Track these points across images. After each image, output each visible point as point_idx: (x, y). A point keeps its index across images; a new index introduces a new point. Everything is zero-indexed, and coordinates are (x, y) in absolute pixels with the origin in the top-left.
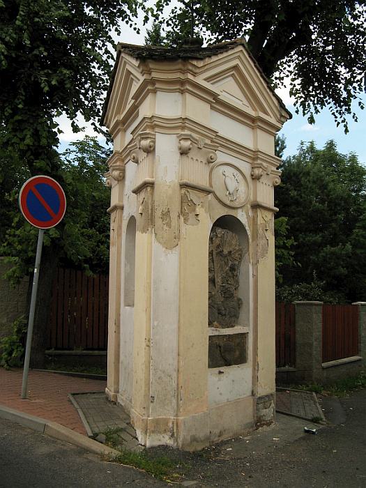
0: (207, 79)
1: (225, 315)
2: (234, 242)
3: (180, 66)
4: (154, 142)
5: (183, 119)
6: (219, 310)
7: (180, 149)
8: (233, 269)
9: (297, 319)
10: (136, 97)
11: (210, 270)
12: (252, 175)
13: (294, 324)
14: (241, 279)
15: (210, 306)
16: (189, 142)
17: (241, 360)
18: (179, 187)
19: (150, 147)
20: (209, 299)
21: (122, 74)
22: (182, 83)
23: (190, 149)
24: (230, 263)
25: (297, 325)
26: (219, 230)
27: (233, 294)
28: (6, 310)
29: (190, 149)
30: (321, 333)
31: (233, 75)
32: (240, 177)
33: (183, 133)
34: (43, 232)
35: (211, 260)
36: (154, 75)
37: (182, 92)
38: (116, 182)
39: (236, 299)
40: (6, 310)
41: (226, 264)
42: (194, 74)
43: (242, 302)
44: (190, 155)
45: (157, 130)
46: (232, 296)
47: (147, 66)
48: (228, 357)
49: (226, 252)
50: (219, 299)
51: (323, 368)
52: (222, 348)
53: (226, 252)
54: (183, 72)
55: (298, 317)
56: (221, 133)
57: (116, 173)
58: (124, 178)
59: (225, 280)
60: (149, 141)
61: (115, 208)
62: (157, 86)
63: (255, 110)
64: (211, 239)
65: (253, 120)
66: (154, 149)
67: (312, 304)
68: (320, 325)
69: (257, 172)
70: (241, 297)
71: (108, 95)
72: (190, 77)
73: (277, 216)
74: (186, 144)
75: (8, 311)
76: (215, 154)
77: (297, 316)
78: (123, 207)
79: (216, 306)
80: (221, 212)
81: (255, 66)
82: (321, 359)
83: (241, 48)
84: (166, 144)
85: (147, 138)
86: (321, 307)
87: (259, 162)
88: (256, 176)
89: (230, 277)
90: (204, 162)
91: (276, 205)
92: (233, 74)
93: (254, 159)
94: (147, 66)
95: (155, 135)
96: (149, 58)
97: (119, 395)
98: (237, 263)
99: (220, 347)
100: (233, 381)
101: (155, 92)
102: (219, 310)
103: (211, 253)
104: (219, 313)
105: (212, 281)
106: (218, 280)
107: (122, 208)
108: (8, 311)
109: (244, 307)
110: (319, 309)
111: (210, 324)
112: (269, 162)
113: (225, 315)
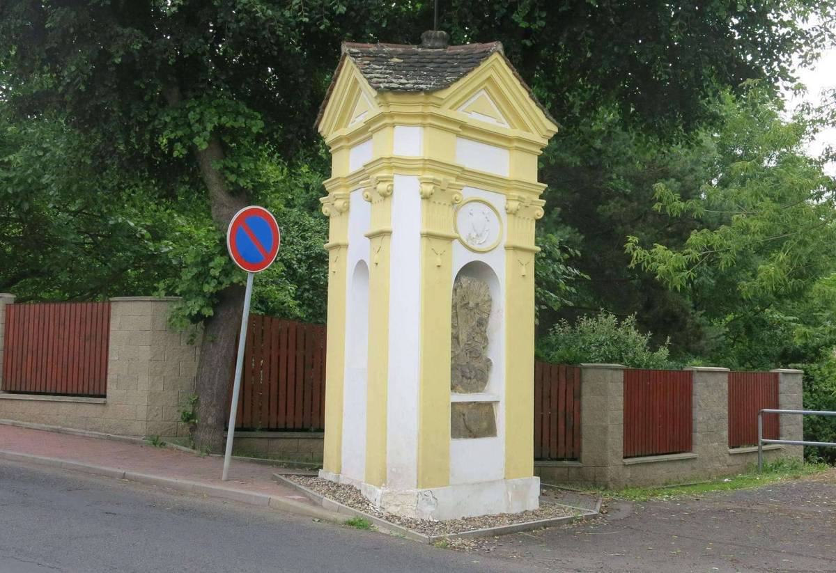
1: (470, 378)
3: (422, 100)
4: (392, 185)
5: (425, 160)
6: (463, 372)
7: (421, 193)
9: (584, 391)
11: (453, 327)
13: (580, 396)
15: (453, 368)
16: (432, 186)
17: (490, 431)
18: (419, 236)
19: (388, 191)
20: (452, 358)
21: (347, 84)
24: (477, 318)
26: (464, 280)
27: (480, 354)
28: (162, 372)
31: (486, 89)
34: (253, 275)
35: (455, 316)
39: (484, 359)
40: (162, 372)
42: (438, 106)
43: (491, 363)
44: (432, 199)
45: (394, 171)
48: (474, 428)
49: (471, 304)
52: (466, 417)
54: (426, 105)
55: (586, 389)
56: (468, 166)
57: (339, 203)
58: (348, 209)
59: (471, 337)
60: (388, 184)
61: (337, 246)
63: (512, 126)
64: (455, 290)
68: (620, 400)
70: (489, 357)
74: (429, 188)
75: (165, 374)
77: (584, 385)
78: (452, 389)
80: (466, 258)
82: (621, 454)
84: (408, 188)
86: (622, 373)
90: (448, 204)
91: (537, 244)
94: (384, 98)
95: (393, 177)
96: (387, 91)
97: (341, 476)
98: (485, 316)
99: (464, 415)
100: (377, 264)
101: (393, 125)
102: (463, 372)
103: (454, 306)
104: (463, 376)
105: (455, 338)
106: (463, 337)
108: (165, 374)
111: (453, 388)
112: (530, 192)
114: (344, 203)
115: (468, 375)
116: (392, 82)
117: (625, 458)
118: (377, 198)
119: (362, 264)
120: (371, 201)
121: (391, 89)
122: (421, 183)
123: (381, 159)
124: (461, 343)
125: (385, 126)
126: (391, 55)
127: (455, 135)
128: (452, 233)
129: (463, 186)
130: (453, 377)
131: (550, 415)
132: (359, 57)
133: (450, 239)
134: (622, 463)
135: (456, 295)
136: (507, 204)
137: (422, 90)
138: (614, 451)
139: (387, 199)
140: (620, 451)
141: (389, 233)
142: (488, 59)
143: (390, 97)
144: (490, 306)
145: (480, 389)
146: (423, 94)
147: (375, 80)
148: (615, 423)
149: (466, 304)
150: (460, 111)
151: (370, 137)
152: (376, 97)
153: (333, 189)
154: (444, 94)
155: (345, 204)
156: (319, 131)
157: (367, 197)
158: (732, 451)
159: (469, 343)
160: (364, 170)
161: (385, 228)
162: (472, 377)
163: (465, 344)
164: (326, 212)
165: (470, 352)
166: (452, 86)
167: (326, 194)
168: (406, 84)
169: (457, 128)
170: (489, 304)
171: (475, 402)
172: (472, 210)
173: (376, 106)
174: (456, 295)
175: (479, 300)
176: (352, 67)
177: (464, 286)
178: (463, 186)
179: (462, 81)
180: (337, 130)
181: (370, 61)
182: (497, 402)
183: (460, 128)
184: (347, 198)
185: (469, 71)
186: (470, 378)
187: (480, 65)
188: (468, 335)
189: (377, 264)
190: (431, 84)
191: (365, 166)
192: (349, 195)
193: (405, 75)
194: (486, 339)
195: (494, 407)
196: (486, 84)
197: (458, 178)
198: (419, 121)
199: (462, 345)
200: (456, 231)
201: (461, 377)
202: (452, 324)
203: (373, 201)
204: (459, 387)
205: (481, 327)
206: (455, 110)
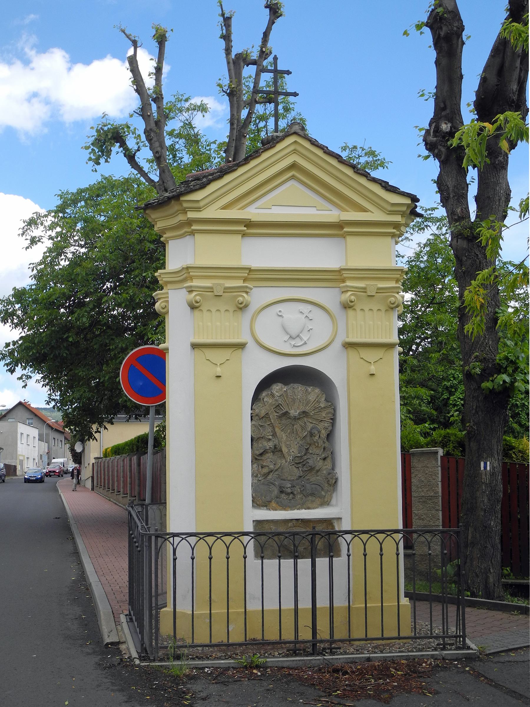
4: (167, 302)
18: (189, 347)
24: (309, 426)
56: (255, 264)
65: (339, 226)
72: (191, 215)
87: (349, 283)
127: (240, 236)
197: (245, 280)
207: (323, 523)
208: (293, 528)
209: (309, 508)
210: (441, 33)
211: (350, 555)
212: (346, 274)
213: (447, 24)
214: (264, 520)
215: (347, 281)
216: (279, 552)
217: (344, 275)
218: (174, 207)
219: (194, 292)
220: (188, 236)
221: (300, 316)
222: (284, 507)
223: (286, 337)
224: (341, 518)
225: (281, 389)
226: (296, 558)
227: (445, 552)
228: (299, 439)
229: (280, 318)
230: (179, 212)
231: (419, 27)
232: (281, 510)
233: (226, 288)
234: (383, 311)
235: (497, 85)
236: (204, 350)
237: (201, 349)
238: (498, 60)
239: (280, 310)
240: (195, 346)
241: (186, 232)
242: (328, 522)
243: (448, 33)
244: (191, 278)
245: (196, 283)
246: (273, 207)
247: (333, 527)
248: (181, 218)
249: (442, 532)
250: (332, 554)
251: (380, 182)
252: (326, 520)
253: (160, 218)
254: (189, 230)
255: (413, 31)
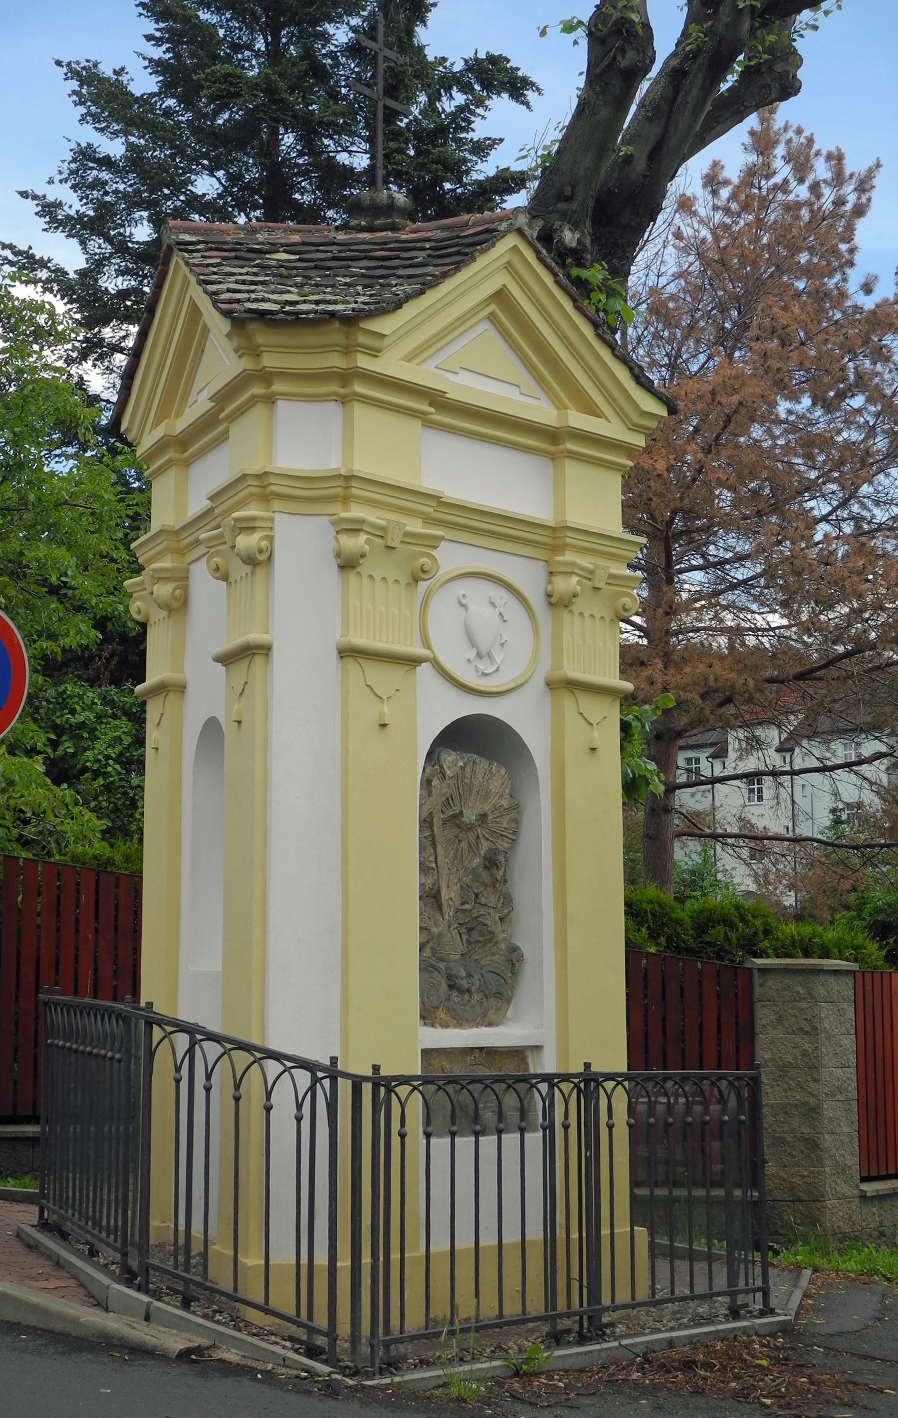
0: (410, 358)
2: (495, 785)
4: (271, 539)
6: (450, 977)
7: (338, 555)
8: (491, 862)
10: (223, 397)
11: (424, 868)
12: (549, 596)
14: (521, 892)
15: (426, 967)
18: (335, 654)
19: (261, 552)
22: (345, 377)
23: (363, 556)
24: (485, 846)
25: (761, 1040)
26: (450, 759)
29: (363, 556)
30: (852, 1073)
32: (514, 609)
33: (344, 515)
36: (270, 361)
37: (345, 400)
38: (164, 613)
39: (503, 946)
41: (473, 849)
45: (277, 505)
46: (490, 938)
47: (248, 337)
49: (470, 815)
50: (454, 946)
51: (864, 1197)
53: (470, 815)
56: (453, 493)
57: (163, 590)
61: (162, 689)
62: (277, 387)
63: (560, 406)
64: (427, 783)
65: (553, 435)
66: (270, 557)
67: (817, 971)
68: (849, 1042)
69: (565, 585)
71: (142, 336)
72: (364, 362)
73: (628, 700)
76: (432, 557)
78: (423, 1017)
79: (442, 965)
81: (558, 283)
83: (511, 241)
85: (253, 529)
86: (850, 981)
87: (569, 556)
88: (561, 598)
89: (485, 885)
92: (492, 314)
93: (556, 549)
95: (272, 520)
96: (251, 319)
98: (503, 844)
100: (239, 722)
101: (270, 400)
102: (450, 977)
103: (426, 823)
104: (451, 987)
107: (181, 688)
109: (528, 971)
110: (845, 988)
111: (428, 1017)
113: (469, 991)
114: (175, 589)
115: (465, 984)
116: (263, 300)
117: (864, 1180)
118: (240, 570)
119: (212, 727)
120: (226, 578)
121: (262, 316)
122: (337, 533)
123: (244, 476)
124: (445, 907)
125: (253, 401)
126: (274, 248)
127: (418, 424)
128: (418, 650)
129: (442, 538)
130: (426, 990)
131: (115, 987)
132: (198, 251)
133: (413, 662)
134: (856, 1192)
135: (430, 795)
136: (550, 582)
137: (333, 315)
138: (837, 1164)
139: (260, 571)
140: (852, 1161)
141: (266, 649)
142: (493, 245)
143: (262, 336)
144: (517, 822)
145: (491, 1016)
146: (337, 325)
147: (225, 296)
148: (839, 1097)
149: (454, 816)
150: (430, 366)
151: (224, 437)
152: (228, 335)
153: (151, 560)
154: (385, 325)
155: (178, 592)
156: (122, 430)
157: (217, 569)
158: (870, 1188)
159: (467, 907)
160: (211, 510)
161: (256, 636)
162: (473, 989)
163: (458, 911)
164: (139, 612)
165: (470, 930)
166: (406, 307)
167: (138, 570)
168: (297, 303)
169: (424, 407)
170: (513, 815)
171: (481, 1049)
172: (464, 596)
173: (233, 356)
174: (430, 795)
175: (487, 808)
176: (186, 277)
177: (449, 773)
178: (442, 538)
179: (431, 297)
180: (157, 425)
181: (224, 258)
182: (538, 1048)
183: (430, 405)
184: (182, 579)
185: (445, 275)
186: (469, 991)
187: (474, 259)
188: (462, 888)
189: (239, 722)
190: (356, 302)
191: (212, 498)
192: (188, 571)
193: (300, 286)
194: (507, 900)
195: (530, 1060)
196: (492, 307)
197: (428, 520)
198: (334, 388)
199: (449, 912)
200: (427, 644)
201: (444, 987)
202: (421, 864)
203: (232, 580)
204: (441, 1014)
205: (494, 871)
206: (418, 364)
207: (514, 1057)
208: (475, 1067)
209: (490, 1024)
210: (619, 59)
211: (569, 1126)
212: (571, 539)
213: (640, 48)
214: (432, 1050)
215: (567, 553)
216: (453, 1122)
217: (567, 539)
218: (335, 334)
219: (362, 533)
220: (332, 404)
221: (489, 610)
222: (460, 1021)
223: (471, 654)
224: (542, 1047)
225: (455, 763)
226: (477, 1134)
227: (743, 1118)
228: (462, 872)
229: (462, 610)
230: (337, 348)
231: (569, 27)
232: (455, 1027)
233: (612, 576)
234: (608, 620)
235: (645, 176)
236: (364, 663)
237: (360, 660)
238: (656, 129)
239: (463, 592)
240: (348, 653)
241: (336, 394)
242: (518, 1053)
243: (637, 66)
244: (346, 500)
245: (356, 512)
246: (462, 372)
247: (527, 1068)
248: (337, 361)
249: (627, 1077)
250: (524, 1124)
251: (632, 365)
252: (517, 1051)
253: (272, 346)
254: (341, 391)
255: (555, 31)
